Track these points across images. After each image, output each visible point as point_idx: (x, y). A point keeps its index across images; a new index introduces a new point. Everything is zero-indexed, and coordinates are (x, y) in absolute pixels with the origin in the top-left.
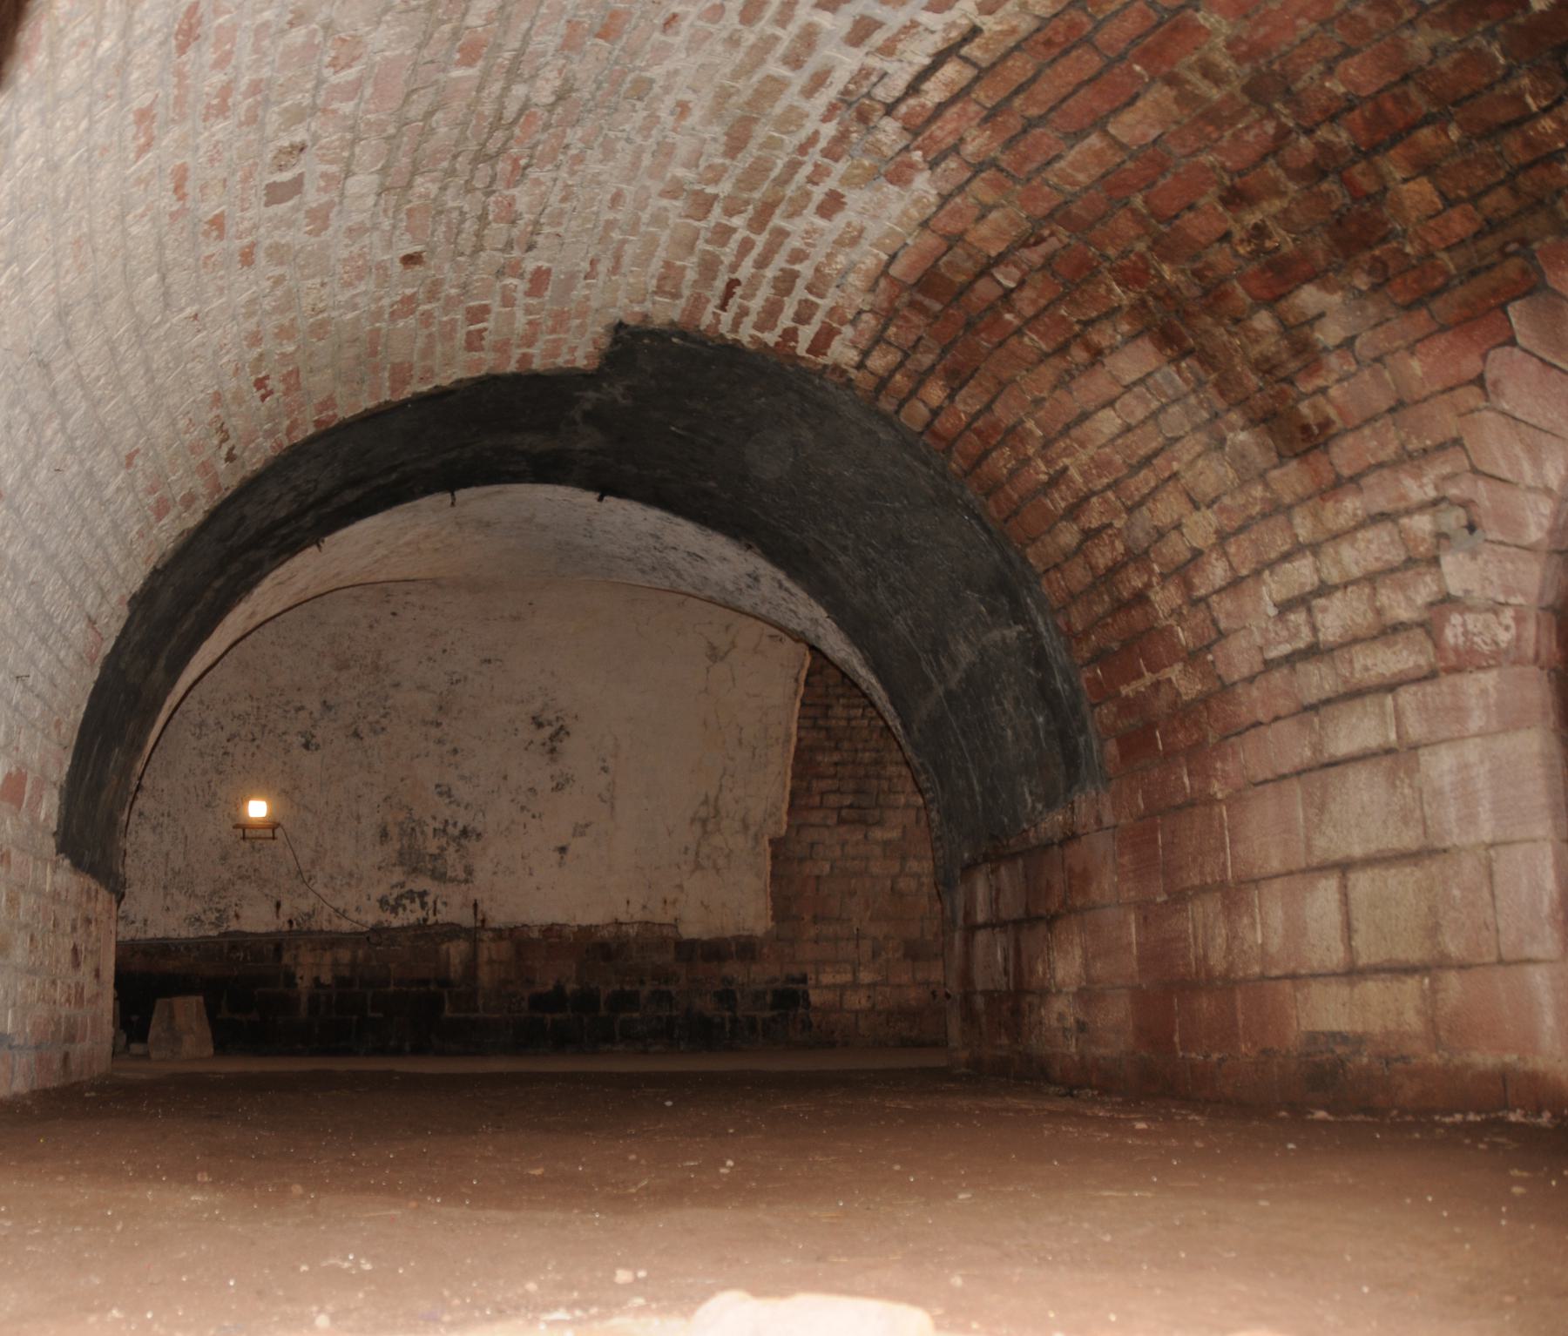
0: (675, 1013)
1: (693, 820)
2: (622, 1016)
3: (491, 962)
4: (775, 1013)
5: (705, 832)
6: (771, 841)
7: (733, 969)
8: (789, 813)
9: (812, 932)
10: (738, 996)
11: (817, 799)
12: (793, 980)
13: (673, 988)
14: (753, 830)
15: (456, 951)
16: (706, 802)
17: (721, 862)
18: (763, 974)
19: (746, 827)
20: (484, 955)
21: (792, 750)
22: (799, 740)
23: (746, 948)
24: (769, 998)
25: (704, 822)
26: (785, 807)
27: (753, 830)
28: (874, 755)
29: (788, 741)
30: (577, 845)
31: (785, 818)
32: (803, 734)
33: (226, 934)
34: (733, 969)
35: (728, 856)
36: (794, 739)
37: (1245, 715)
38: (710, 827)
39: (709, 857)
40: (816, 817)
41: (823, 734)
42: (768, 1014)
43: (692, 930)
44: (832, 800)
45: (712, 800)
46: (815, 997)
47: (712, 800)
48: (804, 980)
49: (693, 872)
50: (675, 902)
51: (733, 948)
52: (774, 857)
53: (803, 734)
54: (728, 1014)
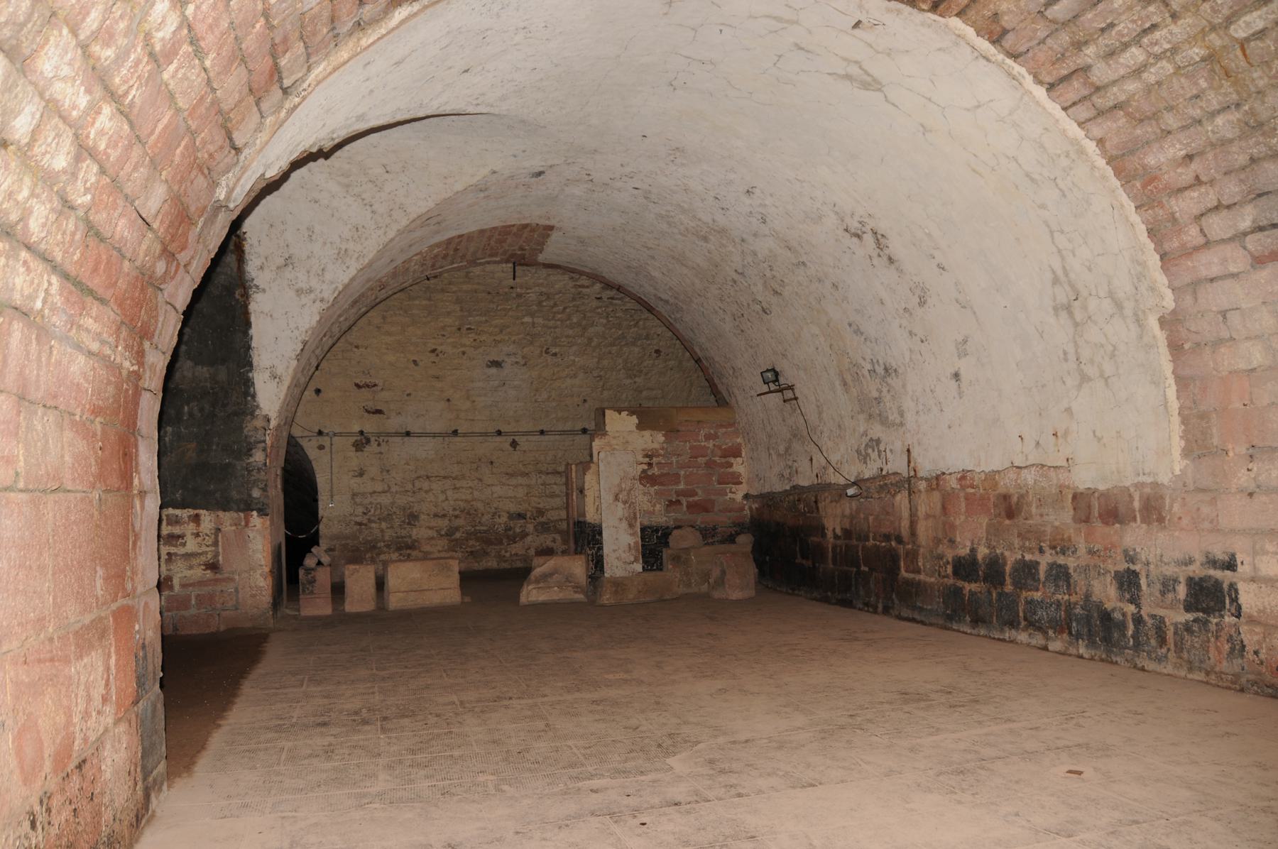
0: (1074, 599)
1: (1056, 309)
2: (1024, 594)
3: (928, 516)
4: (1190, 617)
5: (1076, 325)
6: (1162, 322)
7: (1135, 536)
8: (1165, 268)
9: (1243, 479)
10: (1143, 582)
11: (1193, 231)
12: (1213, 563)
13: (1071, 562)
14: (1129, 307)
15: (927, 504)
16: (1056, 281)
17: (1108, 368)
18: (1166, 551)
19: (1119, 306)
20: (922, 510)
21: (1101, 162)
22: (1101, 142)
23: (1153, 509)
24: (1182, 591)
25: (1068, 308)
26: (1154, 260)
27: (1128, 311)
28: (1234, 116)
29: (1082, 152)
30: (964, 366)
31: (1162, 280)
32: (1097, 131)
33: (794, 487)
34: (1135, 536)
35: (1113, 356)
36: (1091, 147)
37: (27, 52)
38: (1079, 316)
39: (1092, 361)
40: (1209, 263)
41: (1121, 120)
42: (1184, 617)
43: (1084, 478)
44: (1218, 226)
45: (1060, 272)
46: (1249, 598)
47: (1060, 272)
48: (1231, 565)
49: (1080, 387)
50: (1066, 433)
51: (1137, 504)
52: (1176, 348)
53: (1097, 131)
54: (1131, 609)
